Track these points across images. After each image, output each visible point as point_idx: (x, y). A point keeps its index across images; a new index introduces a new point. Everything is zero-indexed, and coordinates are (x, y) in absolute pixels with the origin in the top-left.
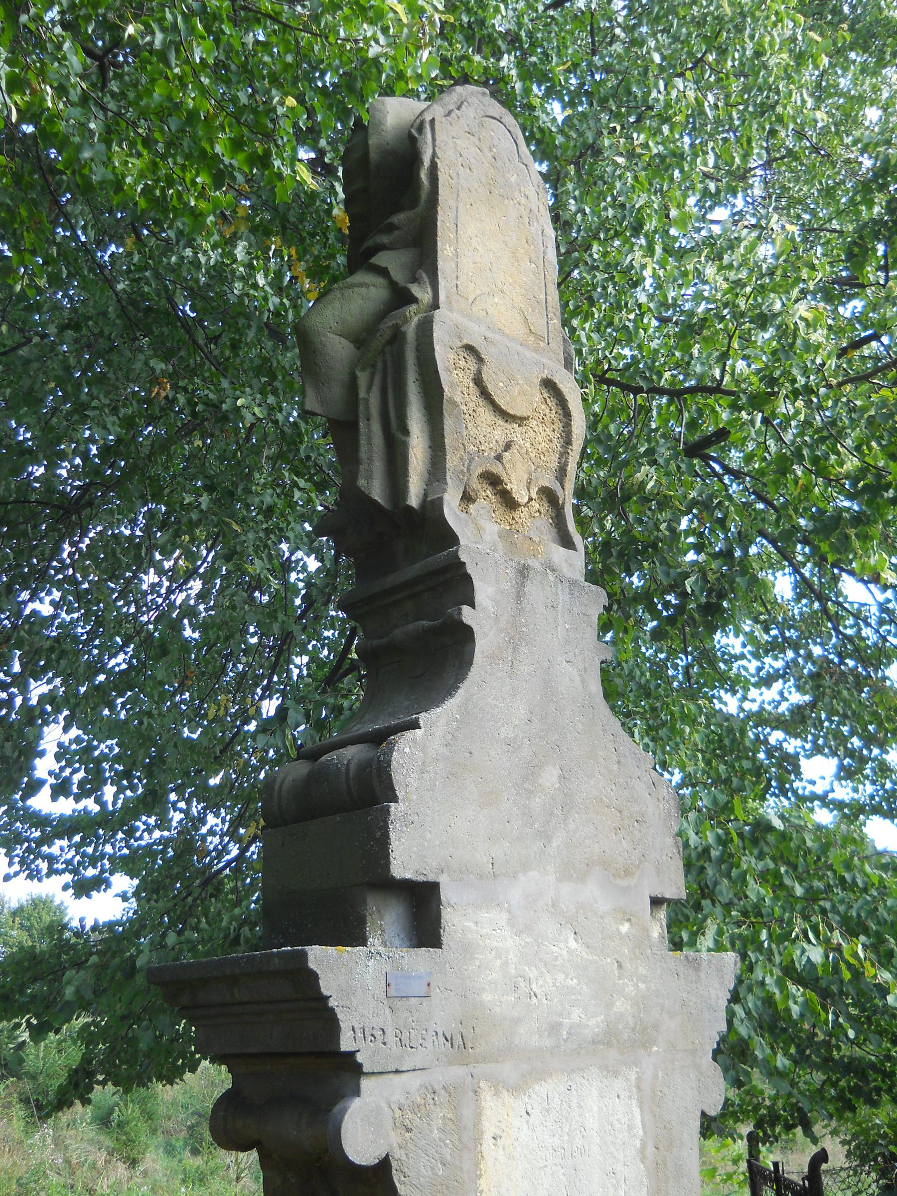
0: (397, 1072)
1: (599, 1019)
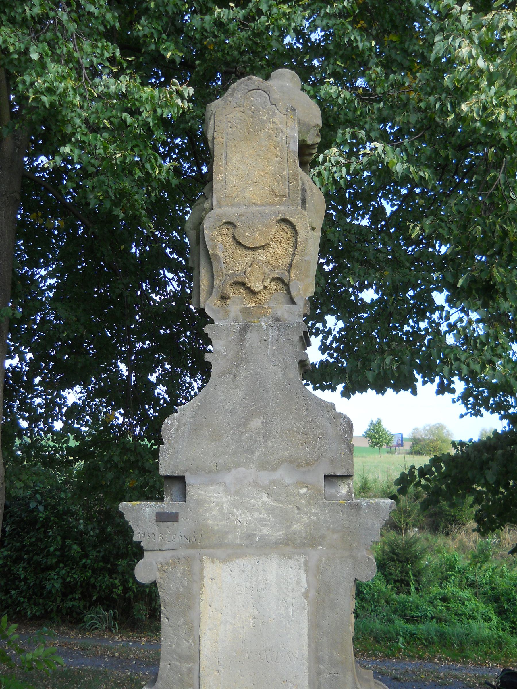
0: (160, 550)
1: (281, 533)
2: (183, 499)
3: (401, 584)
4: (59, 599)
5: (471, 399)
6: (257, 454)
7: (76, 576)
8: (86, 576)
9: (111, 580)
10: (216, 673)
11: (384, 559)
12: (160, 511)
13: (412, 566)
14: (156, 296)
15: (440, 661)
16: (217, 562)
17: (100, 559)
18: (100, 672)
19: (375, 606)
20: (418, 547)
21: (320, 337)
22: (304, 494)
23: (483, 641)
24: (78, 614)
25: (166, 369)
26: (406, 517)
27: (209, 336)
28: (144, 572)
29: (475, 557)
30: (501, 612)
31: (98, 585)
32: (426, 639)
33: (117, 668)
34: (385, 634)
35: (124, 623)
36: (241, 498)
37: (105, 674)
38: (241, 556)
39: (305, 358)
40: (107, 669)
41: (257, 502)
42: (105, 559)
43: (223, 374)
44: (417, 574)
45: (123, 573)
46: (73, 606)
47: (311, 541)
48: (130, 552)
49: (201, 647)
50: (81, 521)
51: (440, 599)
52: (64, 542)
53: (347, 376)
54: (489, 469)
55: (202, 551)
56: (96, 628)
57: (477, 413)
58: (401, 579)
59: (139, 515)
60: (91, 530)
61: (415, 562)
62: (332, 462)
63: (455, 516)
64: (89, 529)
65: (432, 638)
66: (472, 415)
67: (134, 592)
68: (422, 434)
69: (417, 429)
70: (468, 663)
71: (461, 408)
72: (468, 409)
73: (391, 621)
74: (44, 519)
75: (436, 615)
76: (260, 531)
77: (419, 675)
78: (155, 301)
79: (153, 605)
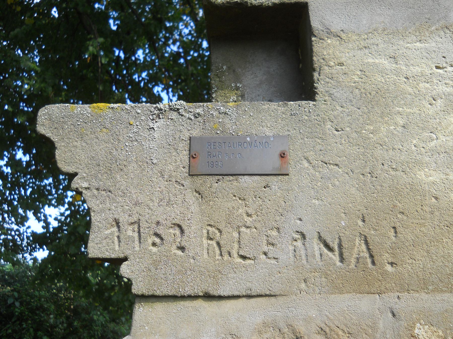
0: (208, 297)
50: (52, 316)
64: (58, 323)
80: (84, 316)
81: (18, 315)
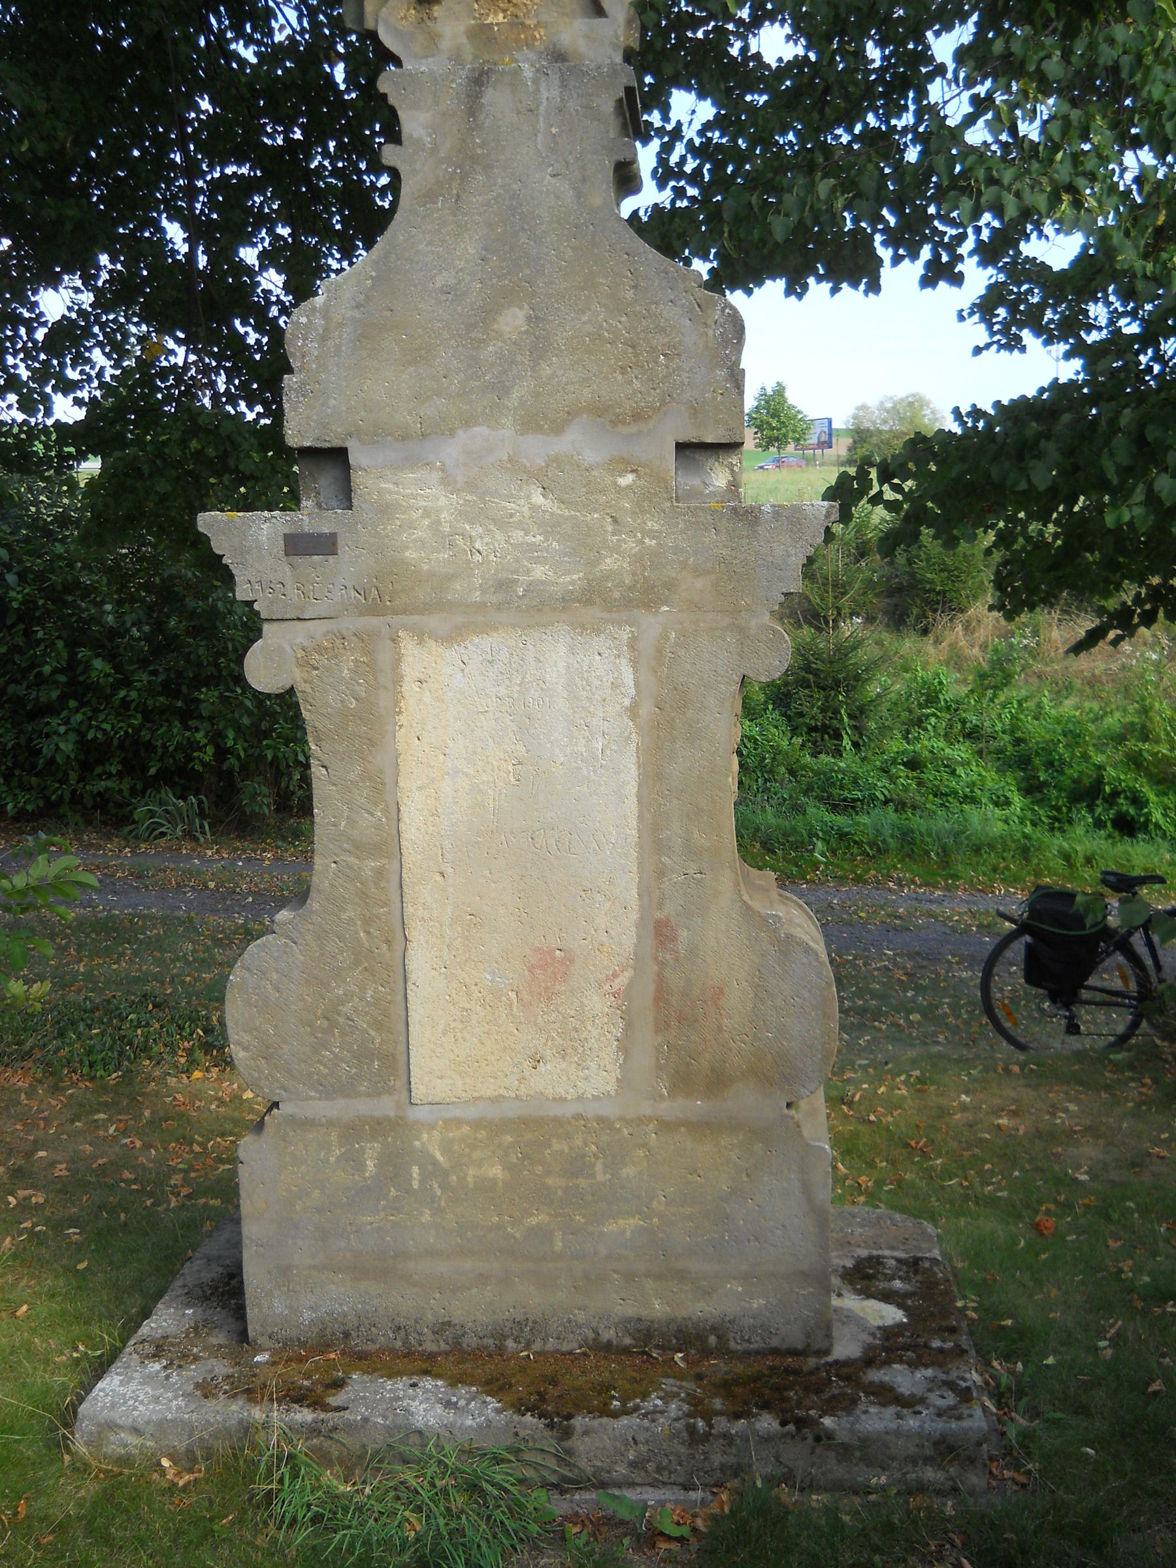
1: (575, 577)
2: (347, 504)
3: (823, 735)
4: (73, 776)
5: (1002, 312)
6: (515, 395)
7: (107, 727)
8: (129, 725)
9: (188, 734)
10: (439, 878)
11: (786, 684)
12: (292, 531)
13: (847, 697)
14: (246, 46)
15: (901, 885)
16: (431, 643)
17: (159, 689)
18: (178, 919)
19: (766, 781)
20: (864, 655)
21: (655, 145)
22: (629, 487)
23: (989, 845)
24: (120, 806)
25: (281, 237)
26: (835, 597)
27: (392, 101)
28: (264, 669)
29: (982, 676)
30: (1031, 788)
31: (159, 743)
32: (872, 844)
33: (214, 911)
34: (785, 835)
35: (222, 822)
36: (482, 498)
37: (189, 923)
38: (486, 628)
39: (629, 157)
40: (193, 914)
41: (518, 507)
42: (169, 689)
43: (429, 196)
44: (857, 713)
45: (211, 719)
46: (107, 789)
47: (644, 595)
48: (224, 673)
49: (402, 827)
50: (108, 607)
51: (904, 764)
52: (72, 655)
53: (726, 229)
54: (1039, 456)
55: (396, 620)
56: (163, 834)
57: (1014, 344)
58: (824, 725)
59: (248, 540)
60: (133, 625)
61: (854, 687)
62: (695, 412)
63: (945, 592)
64: (128, 625)
65: (884, 842)
66: (1001, 347)
67: (238, 757)
68: (876, 420)
69: (863, 407)
70: (958, 887)
71: (978, 333)
72: (993, 334)
73: (799, 809)
74: (22, 603)
75: (895, 796)
76: (528, 572)
77: (855, 913)
78: (243, 62)
79: (283, 785)
80: (191, 603)
81: (19, 609)
